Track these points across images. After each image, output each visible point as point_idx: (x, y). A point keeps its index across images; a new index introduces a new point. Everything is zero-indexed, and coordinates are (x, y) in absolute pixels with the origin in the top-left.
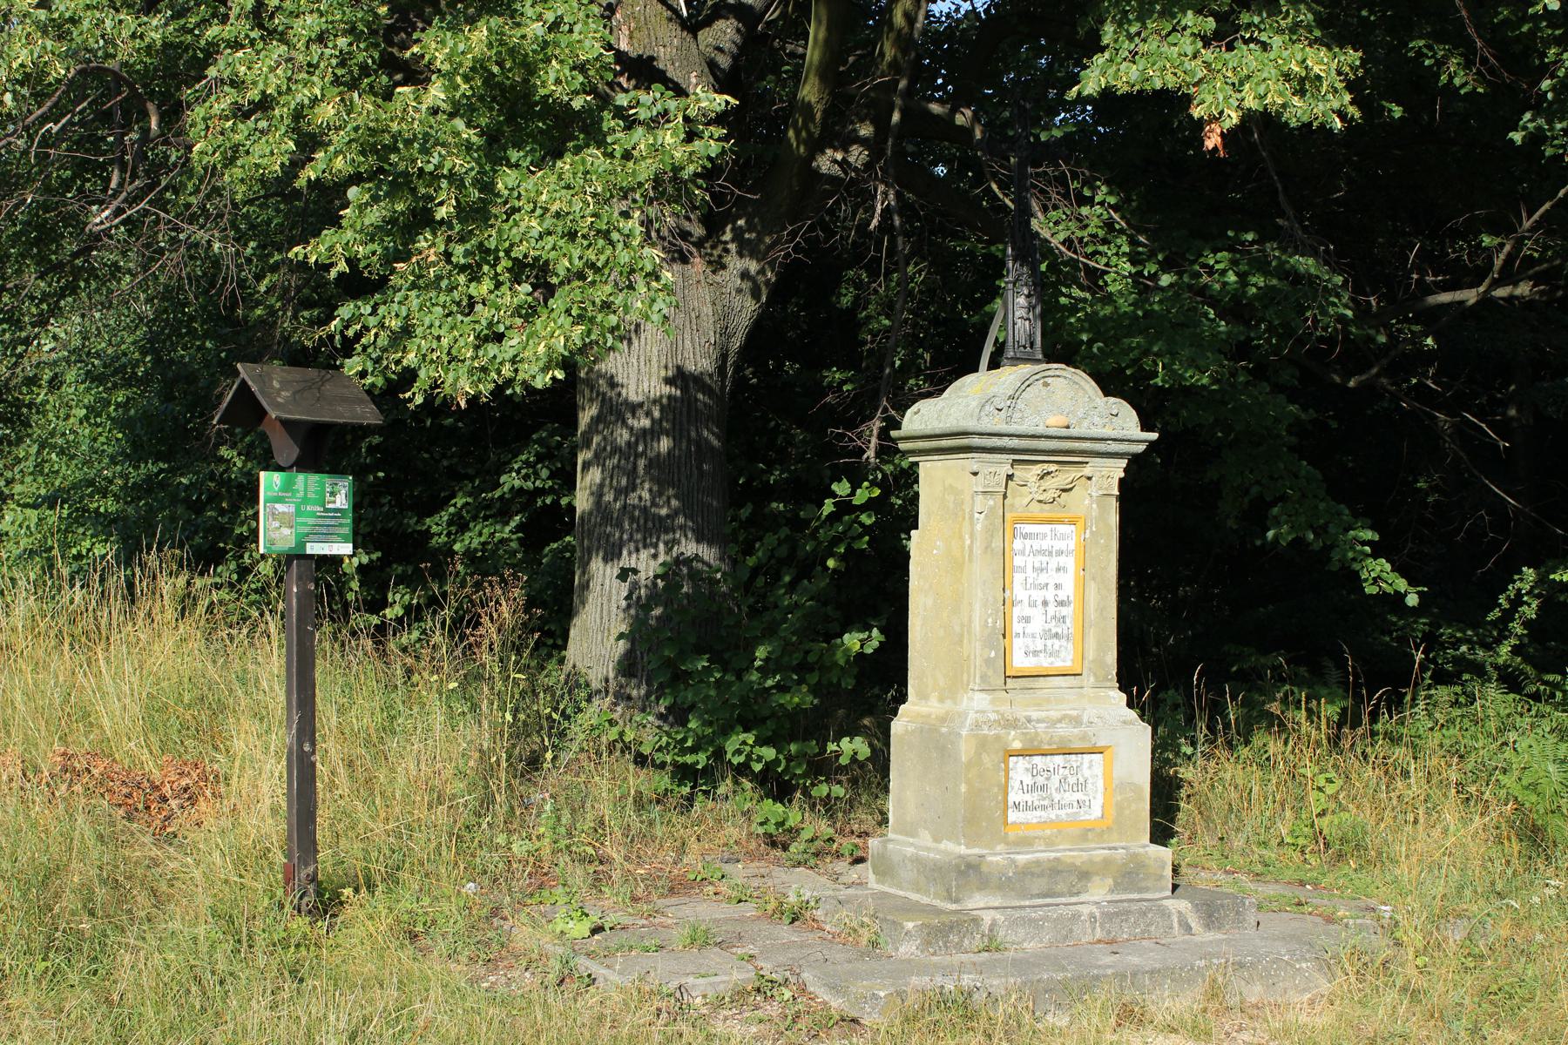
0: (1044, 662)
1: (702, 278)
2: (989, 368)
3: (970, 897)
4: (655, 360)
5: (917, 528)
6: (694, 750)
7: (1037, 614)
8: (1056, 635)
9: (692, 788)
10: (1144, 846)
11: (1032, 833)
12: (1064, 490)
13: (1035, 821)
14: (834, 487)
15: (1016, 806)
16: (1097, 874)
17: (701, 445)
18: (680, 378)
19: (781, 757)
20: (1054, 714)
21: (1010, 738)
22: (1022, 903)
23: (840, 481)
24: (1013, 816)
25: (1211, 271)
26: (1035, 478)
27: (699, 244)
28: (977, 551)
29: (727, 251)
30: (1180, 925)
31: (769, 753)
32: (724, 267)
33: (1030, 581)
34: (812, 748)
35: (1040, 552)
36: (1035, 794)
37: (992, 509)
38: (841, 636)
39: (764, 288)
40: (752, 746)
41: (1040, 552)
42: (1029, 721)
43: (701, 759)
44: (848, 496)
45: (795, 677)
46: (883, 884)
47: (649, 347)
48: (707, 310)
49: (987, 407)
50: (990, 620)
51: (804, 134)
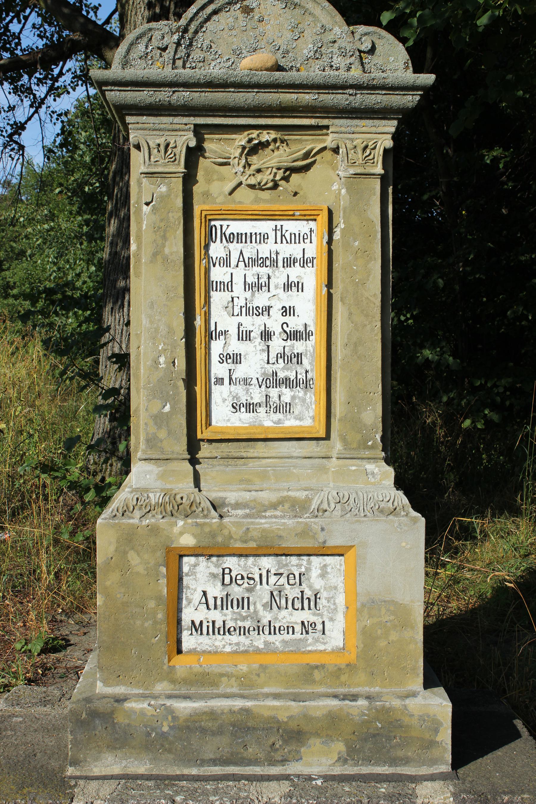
3: (97, 759)
8: (287, 382)
13: (228, 649)
16: (317, 735)
20: (266, 496)
21: (176, 530)
22: (186, 771)
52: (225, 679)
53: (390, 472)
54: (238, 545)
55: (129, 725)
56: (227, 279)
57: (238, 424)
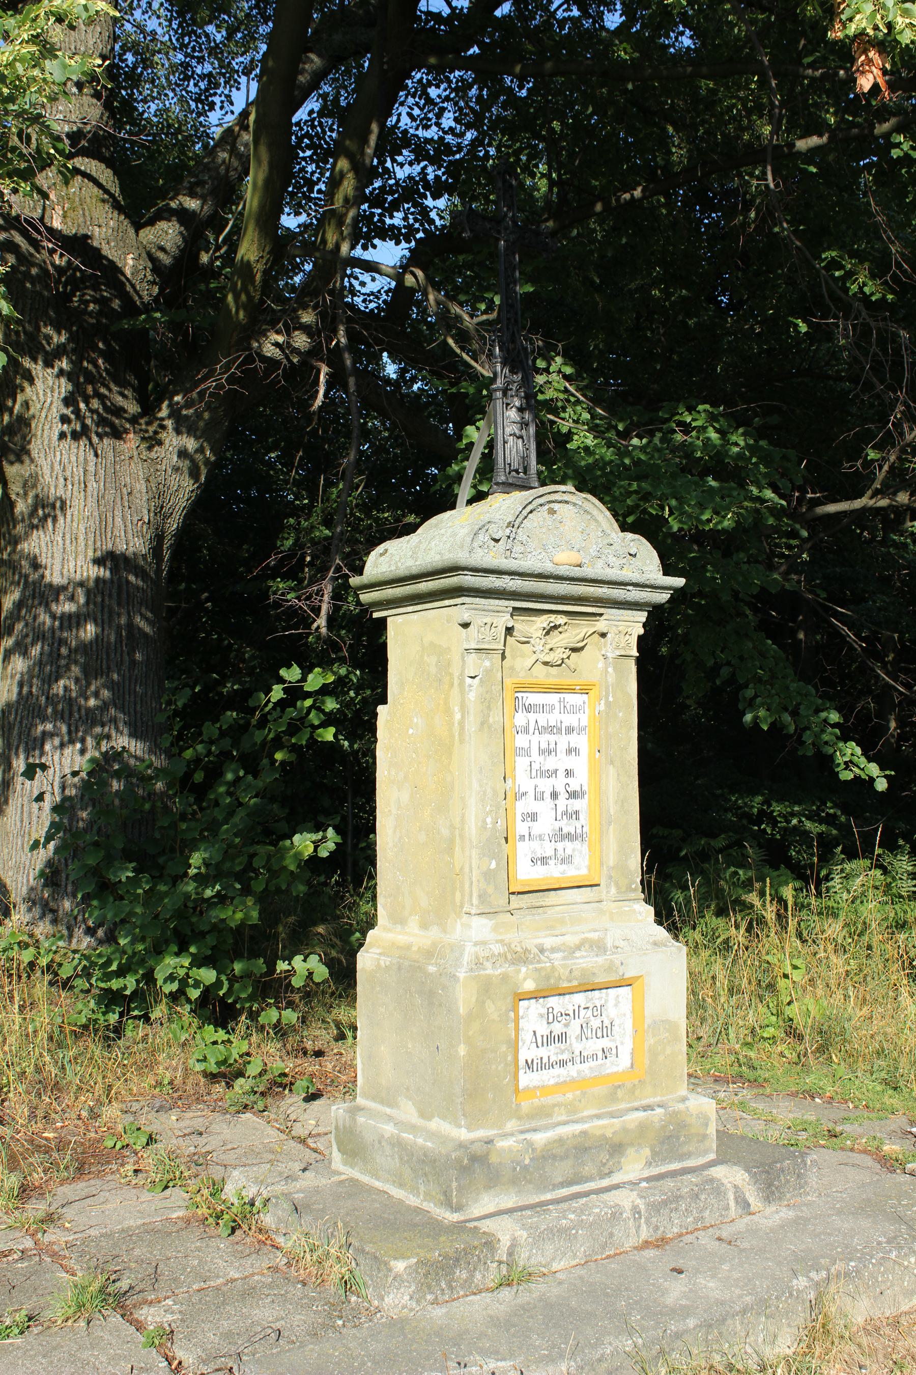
0: (554, 872)
1: (135, 453)
2: (470, 502)
4: (81, 537)
5: (385, 702)
6: (121, 972)
7: (544, 809)
8: (569, 837)
9: (121, 1015)
10: (684, 1099)
11: (550, 1100)
12: (574, 650)
13: (552, 1082)
14: (283, 672)
15: (529, 1065)
16: (632, 1144)
17: (133, 635)
18: (107, 559)
19: (223, 978)
20: (572, 940)
21: (521, 976)
23: (289, 666)
24: (526, 1079)
25: (686, 428)
26: (540, 633)
27: (134, 420)
28: (472, 725)
29: (163, 427)
30: (737, 1202)
31: (208, 975)
32: (160, 443)
33: (535, 766)
34: (260, 968)
35: (550, 729)
36: (552, 1048)
37: (488, 672)
38: (290, 837)
39: (203, 467)
40: (189, 969)
41: (550, 729)
42: (542, 951)
43: (130, 983)
44: (298, 682)
45: (238, 886)
46: (352, 1167)
47: (75, 524)
48: (141, 486)
49: (481, 537)
50: (489, 820)
51: (243, 297)
52: (556, 1109)
53: (651, 910)
54: (566, 985)
55: (500, 1163)
56: (526, 746)
57: (536, 876)
